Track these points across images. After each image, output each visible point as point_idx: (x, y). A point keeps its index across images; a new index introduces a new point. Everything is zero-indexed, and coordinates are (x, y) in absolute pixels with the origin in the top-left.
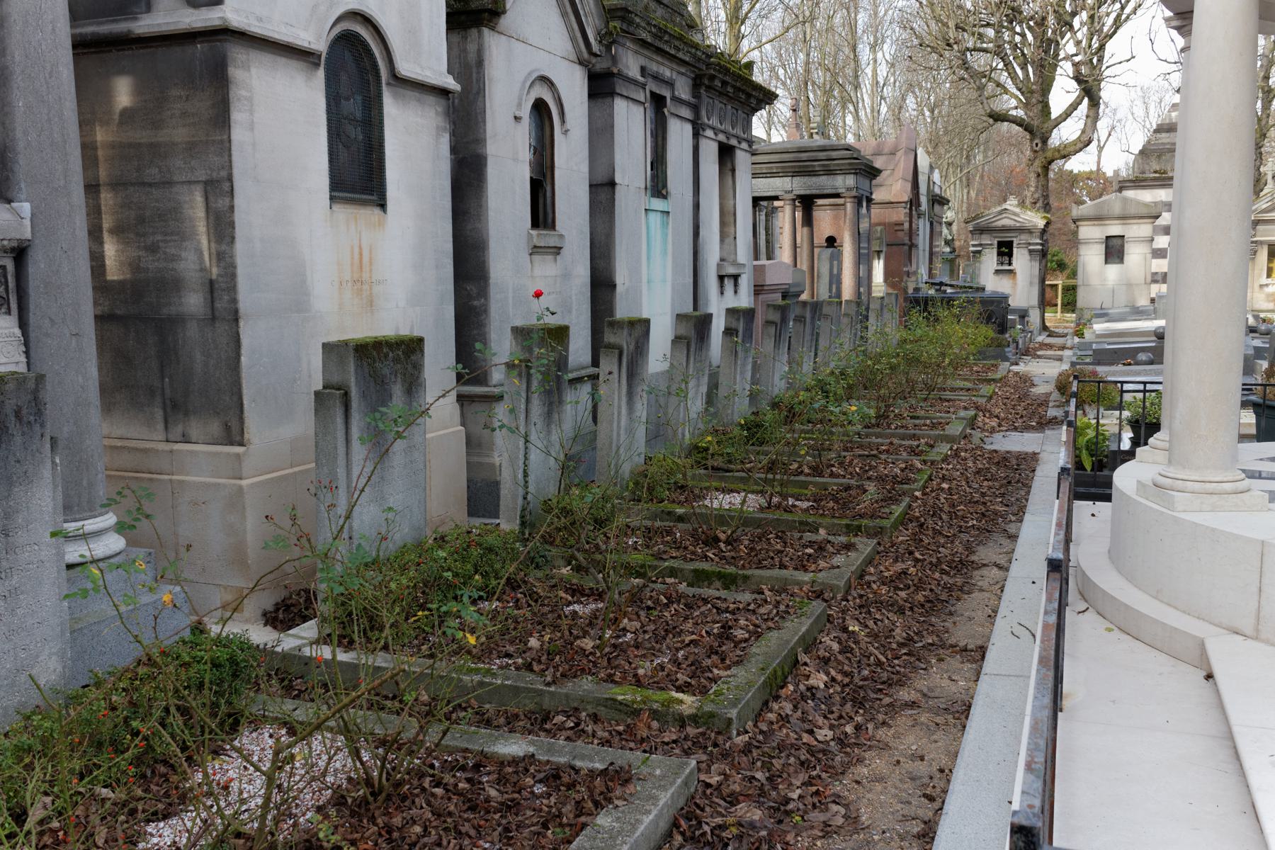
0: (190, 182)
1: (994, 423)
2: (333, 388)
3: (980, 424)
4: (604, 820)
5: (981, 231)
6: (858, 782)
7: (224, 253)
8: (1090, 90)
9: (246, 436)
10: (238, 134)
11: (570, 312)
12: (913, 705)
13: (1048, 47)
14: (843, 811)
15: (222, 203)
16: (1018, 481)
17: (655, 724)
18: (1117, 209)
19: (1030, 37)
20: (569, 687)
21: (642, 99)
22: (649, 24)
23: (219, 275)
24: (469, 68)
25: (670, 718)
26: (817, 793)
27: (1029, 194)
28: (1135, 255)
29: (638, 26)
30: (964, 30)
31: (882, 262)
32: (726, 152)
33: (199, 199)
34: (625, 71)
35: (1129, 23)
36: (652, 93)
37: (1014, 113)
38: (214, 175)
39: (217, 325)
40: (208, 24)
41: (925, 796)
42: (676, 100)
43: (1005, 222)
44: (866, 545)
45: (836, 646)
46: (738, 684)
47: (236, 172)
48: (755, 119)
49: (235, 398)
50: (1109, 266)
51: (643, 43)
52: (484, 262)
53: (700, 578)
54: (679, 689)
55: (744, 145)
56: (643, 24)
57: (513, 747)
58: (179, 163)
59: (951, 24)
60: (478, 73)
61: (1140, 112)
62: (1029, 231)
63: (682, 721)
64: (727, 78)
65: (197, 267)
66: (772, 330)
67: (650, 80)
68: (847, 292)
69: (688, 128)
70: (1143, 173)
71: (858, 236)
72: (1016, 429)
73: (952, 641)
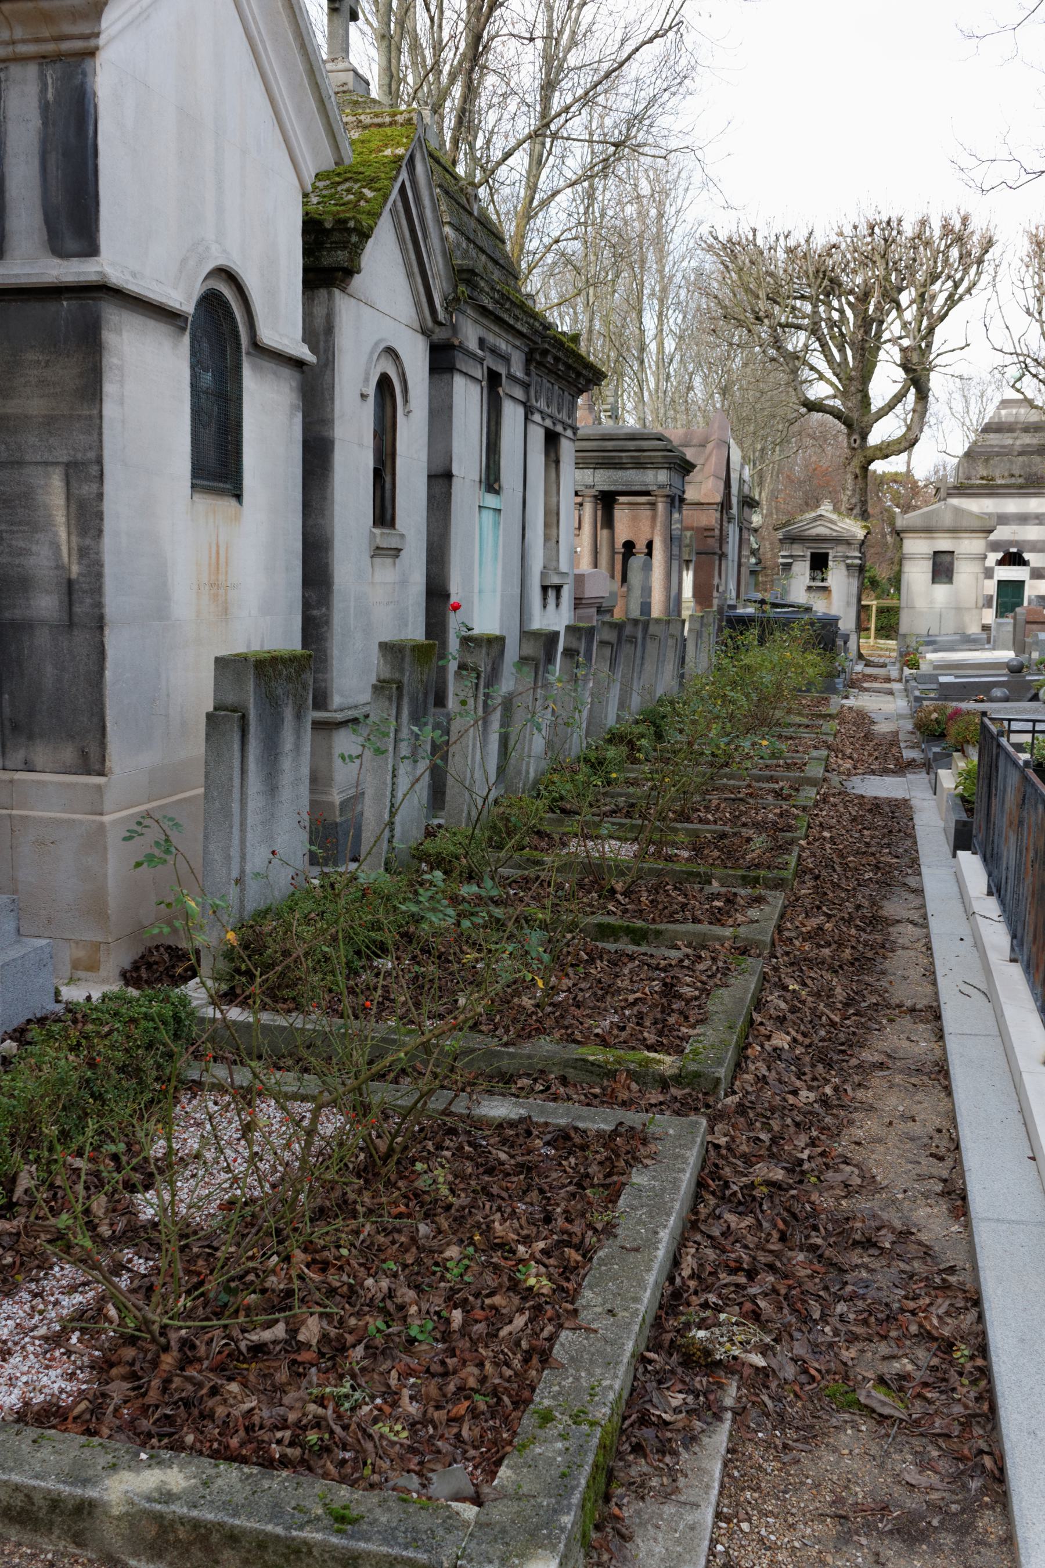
0: (46, 464)
1: (848, 765)
2: (226, 709)
3: (834, 766)
4: (639, 1178)
5: (792, 539)
6: (858, 1144)
7: (88, 548)
8: (917, 376)
9: (107, 763)
10: (110, 410)
11: (406, 625)
12: (881, 1066)
13: (869, 326)
14: (856, 1171)
15: (87, 490)
16: (900, 831)
17: (634, 1086)
18: (948, 521)
19: (849, 313)
20: (527, 1048)
21: (480, 377)
22: (493, 289)
23: (79, 574)
24: (320, 332)
25: (649, 1079)
26: (823, 1154)
27: (845, 499)
28: (965, 573)
29: (482, 290)
30: (776, 302)
31: (691, 573)
32: (552, 439)
33: (56, 482)
34: (466, 343)
35: (961, 304)
36: (489, 368)
37: (830, 402)
38: (79, 456)
39: (76, 633)
40: (82, 278)
41: (932, 1155)
42: (511, 377)
43: (821, 530)
44: (777, 900)
45: (783, 1005)
46: (710, 1042)
47: (106, 454)
48: (580, 401)
49: (95, 720)
50: (937, 586)
51: (484, 311)
52: (327, 565)
53: (605, 932)
54: (650, 1048)
55: (569, 433)
56: (487, 289)
57: (499, 1109)
58: (33, 440)
59: (762, 294)
60: (327, 341)
61: (958, 406)
62: (848, 542)
63: (663, 1083)
64: (560, 354)
65: (53, 564)
66: (607, 652)
67: (488, 354)
68: (657, 611)
69: (520, 411)
70: (969, 478)
71: (671, 540)
72: (873, 772)
73: (895, 1001)
